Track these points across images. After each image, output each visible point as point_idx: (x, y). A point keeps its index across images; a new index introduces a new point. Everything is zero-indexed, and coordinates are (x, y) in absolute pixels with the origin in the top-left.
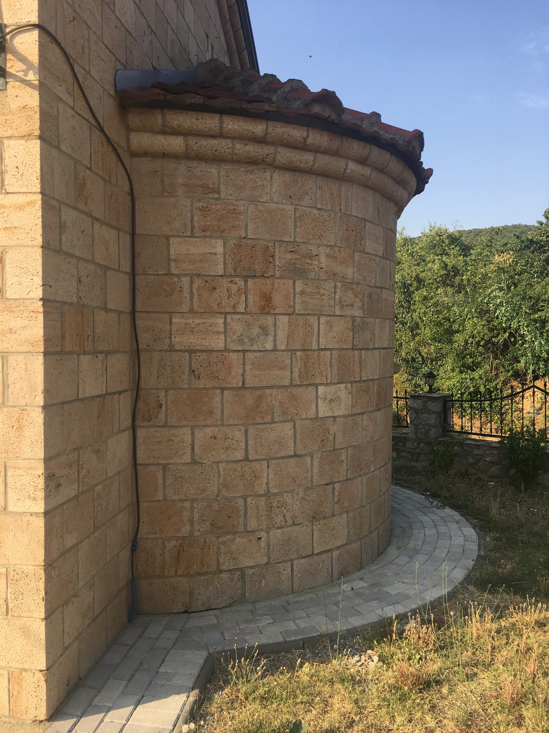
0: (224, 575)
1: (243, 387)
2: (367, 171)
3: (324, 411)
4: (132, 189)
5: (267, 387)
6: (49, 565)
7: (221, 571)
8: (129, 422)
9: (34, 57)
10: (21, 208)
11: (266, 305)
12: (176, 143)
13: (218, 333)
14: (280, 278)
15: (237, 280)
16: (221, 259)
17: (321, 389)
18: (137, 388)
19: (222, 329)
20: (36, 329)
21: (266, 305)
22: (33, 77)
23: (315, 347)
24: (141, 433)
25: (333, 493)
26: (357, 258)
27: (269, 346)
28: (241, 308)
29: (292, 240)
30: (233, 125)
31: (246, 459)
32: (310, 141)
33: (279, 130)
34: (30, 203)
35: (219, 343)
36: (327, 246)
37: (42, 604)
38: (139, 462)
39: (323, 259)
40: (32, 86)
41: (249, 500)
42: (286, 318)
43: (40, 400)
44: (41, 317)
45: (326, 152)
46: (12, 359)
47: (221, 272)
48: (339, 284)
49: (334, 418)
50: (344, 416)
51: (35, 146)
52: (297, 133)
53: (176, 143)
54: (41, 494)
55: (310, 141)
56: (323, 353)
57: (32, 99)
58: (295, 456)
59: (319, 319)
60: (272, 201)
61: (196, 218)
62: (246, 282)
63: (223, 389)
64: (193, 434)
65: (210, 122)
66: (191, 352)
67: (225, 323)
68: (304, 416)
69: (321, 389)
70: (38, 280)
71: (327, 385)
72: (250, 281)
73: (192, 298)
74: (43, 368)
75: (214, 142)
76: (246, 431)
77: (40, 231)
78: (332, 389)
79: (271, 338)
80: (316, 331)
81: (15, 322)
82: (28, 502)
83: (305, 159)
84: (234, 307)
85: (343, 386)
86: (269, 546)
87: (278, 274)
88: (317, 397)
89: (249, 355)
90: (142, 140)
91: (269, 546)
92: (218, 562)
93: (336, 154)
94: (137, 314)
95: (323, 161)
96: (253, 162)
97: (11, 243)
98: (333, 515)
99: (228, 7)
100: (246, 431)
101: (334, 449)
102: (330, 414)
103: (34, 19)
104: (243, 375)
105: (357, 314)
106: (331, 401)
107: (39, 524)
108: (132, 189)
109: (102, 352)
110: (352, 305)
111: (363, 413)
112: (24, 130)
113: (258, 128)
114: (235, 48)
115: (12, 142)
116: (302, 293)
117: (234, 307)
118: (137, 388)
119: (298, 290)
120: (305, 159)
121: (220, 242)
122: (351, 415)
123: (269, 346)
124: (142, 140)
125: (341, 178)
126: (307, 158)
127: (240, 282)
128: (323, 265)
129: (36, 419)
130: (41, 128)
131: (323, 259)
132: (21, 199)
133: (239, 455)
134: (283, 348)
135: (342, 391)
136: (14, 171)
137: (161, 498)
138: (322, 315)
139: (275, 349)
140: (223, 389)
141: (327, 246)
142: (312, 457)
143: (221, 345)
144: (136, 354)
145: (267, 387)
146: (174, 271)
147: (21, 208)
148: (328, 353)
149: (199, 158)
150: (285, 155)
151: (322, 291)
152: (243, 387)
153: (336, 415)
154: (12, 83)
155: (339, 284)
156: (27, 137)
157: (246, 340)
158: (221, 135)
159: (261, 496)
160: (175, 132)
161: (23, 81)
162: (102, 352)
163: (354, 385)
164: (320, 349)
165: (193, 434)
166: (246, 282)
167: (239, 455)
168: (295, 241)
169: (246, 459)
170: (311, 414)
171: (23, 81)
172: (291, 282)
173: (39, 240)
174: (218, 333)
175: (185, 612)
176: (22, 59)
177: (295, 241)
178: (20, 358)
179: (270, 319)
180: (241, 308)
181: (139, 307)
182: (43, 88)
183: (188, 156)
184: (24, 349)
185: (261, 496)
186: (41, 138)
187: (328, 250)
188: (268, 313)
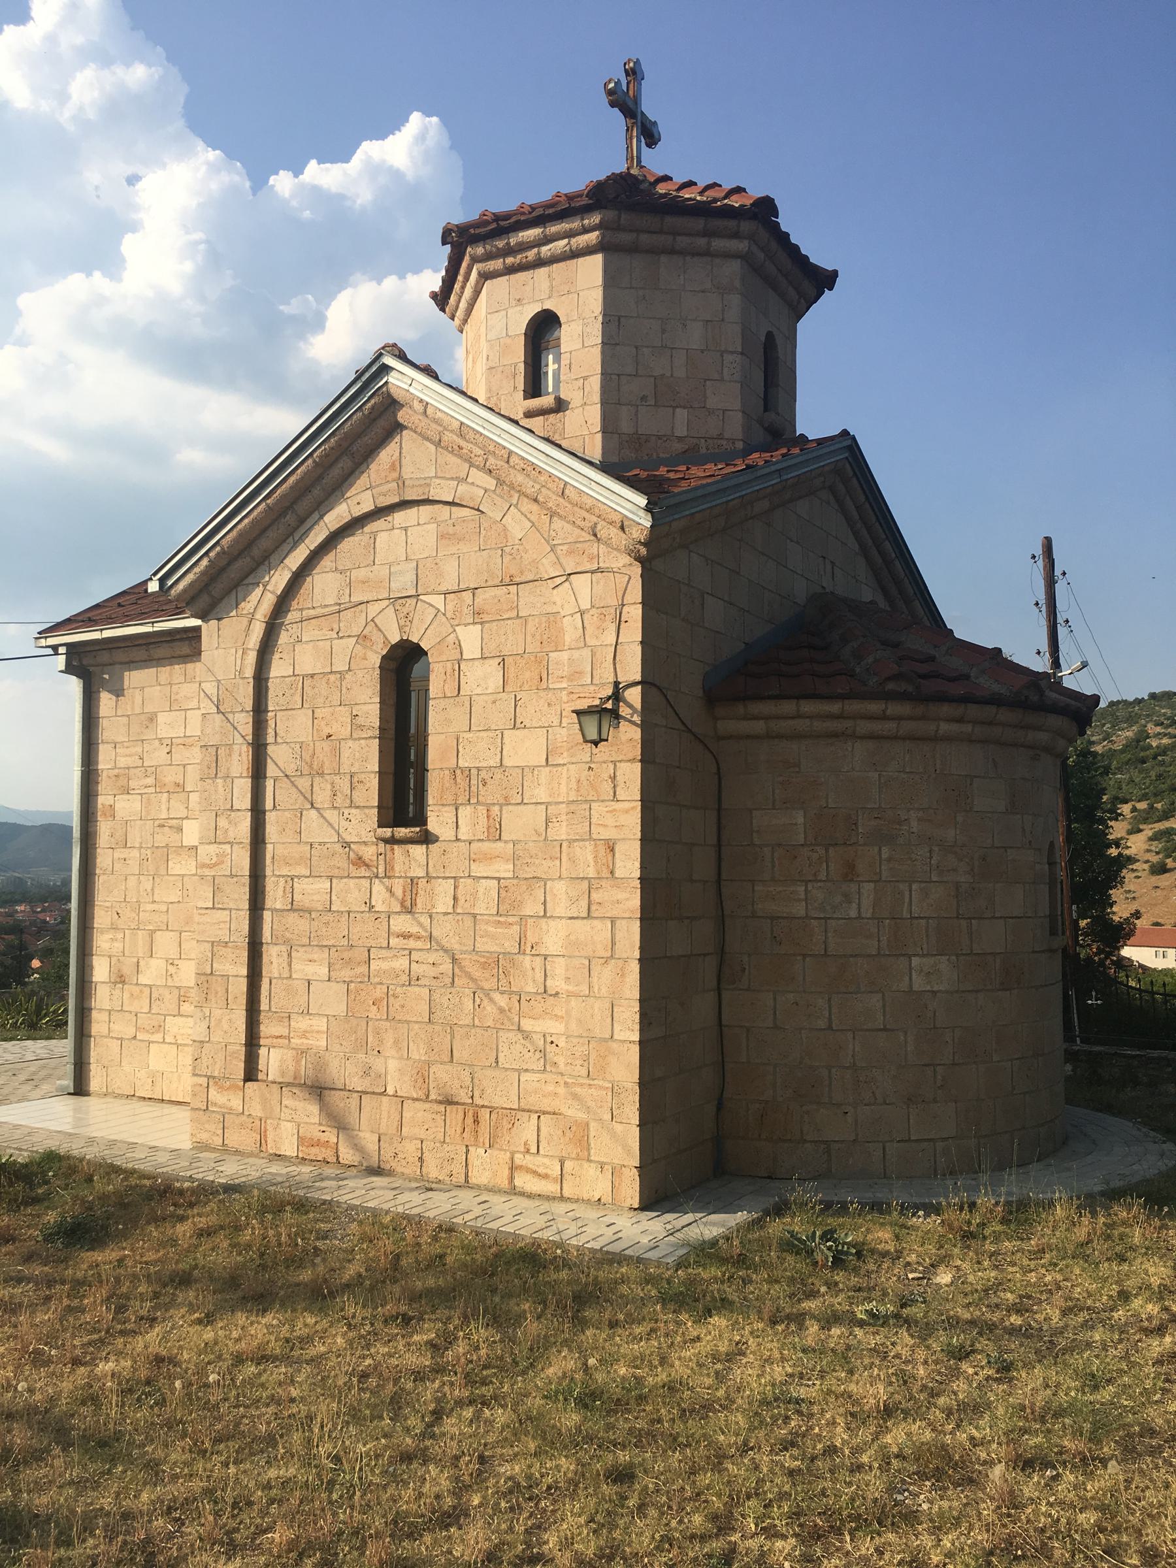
0: (807, 1145)
1: (826, 955)
2: (968, 728)
3: (919, 983)
4: (719, 769)
5: (851, 956)
6: (642, 1084)
7: (805, 1141)
8: (715, 983)
9: (638, 705)
10: (627, 812)
11: (849, 872)
12: (759, 727)
13: (799, 900)
14: (865, 845)
15: (818, 848)
16: (802, 830)
17: (915, 961)
18: (722, 952)
19: (803, 897)
20: (635, 901)
21: (849, 872)
22: (637, 719)
23: (906, 914)
24: (726, 995)
25: (935, 1077)
26: (960, 819)
27: (853, 913)
28: (822, 876)
29: (877, 806)
30: (808, 707)
31: (830, 1028)
32: (889, 712)
33: (855, 706)
34: (633, 808)
35: (800, 910)
36: (919, 809)
37: (637, 1113)
38: (724, 1022)
39: (914, 824)
40: (636, 725)
41: (834, 1070)
42: (872, 885)
43: (637, 954)
44: (639, 891)
45: (910, 718)
46: (618, 922)
47: (802, 841)
48: (936, 849)
49: (934, 992)
50: (947, 992)
51: (638, 766)
52: (874, 707)
53: (759, 727)
54: (637, 1027)
55: (889, 712)
56: (915, 922)
57: (636, 733)
58: (885, 1029)
59: (910, 886)
60: (853, 769)
61: (777, 791)
62: (827, 851)
63: (804, 956)
64: (775, 999)
65: (788, 707)
66: (772, 918)
67: (806, 890)
68: (894, 988)
69: (915, 961)
70: (638, 864)
71: (923, 956)
72: (831, 850)
73: (773, 867)
74: (623, 820)
75: (791, 722)
76: (829, 1000)
77: (639, 828)
78: (930, 961)
79: (854, 905)
80: (907, 900)
81: (621, 896)
82: (628, 1033)
83: (890, 727)
84: (815, 875)
85: (945, 958)
86: (856, 1121)
87: (861, 841)
88: (911, 969)
89: (833, 923)
90: (728, 726)
91: (856, 1121)
92: (802, 1131)
93: (923, 718)
94: (723, 883)
95: (908, 727)
96: (835, 735)
97: (619, 837)
98: (935, 1101)
99: (857, 507)
100: (829, 1000)
101: (935, 1028)
102: (928, 988)
103: (638, 678)
104: (825, 942)
105: (963, 880)
106: (928, 974)
107: (636, 1050)
108: (719, 769)
109: (688, 918)
110: (955, 870)
111: (977, 991)
112: (630, 756)
113: (835, 707)
114: (870, 542)
115: (622, 764)
116: (889, 860)
117: (815, 875)
118: (722, 952)
119: (884, 856)
120: (890, 727)
121: (801, 813)
122: (957, 992)
123: (853, 913)
124: (728, 726)
125: (935, 739)
126: (891, 726)
127: (821, 851)
128: (915, 830)
129: (635, 967)
130: (642, 754)
131: (914, 824)
132: (627, 805)
133: (822, 1024)
134: (869, 915)
135: (943, 963)
136: (622, 785)
137: (744, 1060)
138: (914, 882)
139: (860, 917)
140: (804, 956)
141: (919, 809)
142: (906, 1033)
143: (802, 913)
144: (721, 921)
145: (851, 956)
146: (757, 841)
147: (627, 812)
148: (923, 922)
149: (780, 736)
150: (864, 727)
151: (913, 856)
152: (826, 955)
153: (935, 989)
154: (622, 723)
155: (936, 849)
156: (632, 760)
157: (828, 908)
158: (799, 716)
159: (847, 1068)
160: (756, 718)
161: (630, 721)
162: (688, 918)
163: (962, 958)
164: (912, 918)
165: (775, 999)
166: (827, 851)
167: (822, 1024)
168: (880, 807)
169: (830, 1028)
170: (904, 986)
171: (630, 721)
172: (876, 849)
173: (639, 835)
174: (799, 900)
175: (770, 1177)
176: (630, 706)
177: (880, 807)
178: (624, 922)
179: (853, 887)
180: (822, 876)
181: (724, 876)
182: (645, 726)
183: (769, 736)
184: (627, 915)
185: (847, 1068)
186: (641, 761)
187: (920, 814)
188: (852, 880)
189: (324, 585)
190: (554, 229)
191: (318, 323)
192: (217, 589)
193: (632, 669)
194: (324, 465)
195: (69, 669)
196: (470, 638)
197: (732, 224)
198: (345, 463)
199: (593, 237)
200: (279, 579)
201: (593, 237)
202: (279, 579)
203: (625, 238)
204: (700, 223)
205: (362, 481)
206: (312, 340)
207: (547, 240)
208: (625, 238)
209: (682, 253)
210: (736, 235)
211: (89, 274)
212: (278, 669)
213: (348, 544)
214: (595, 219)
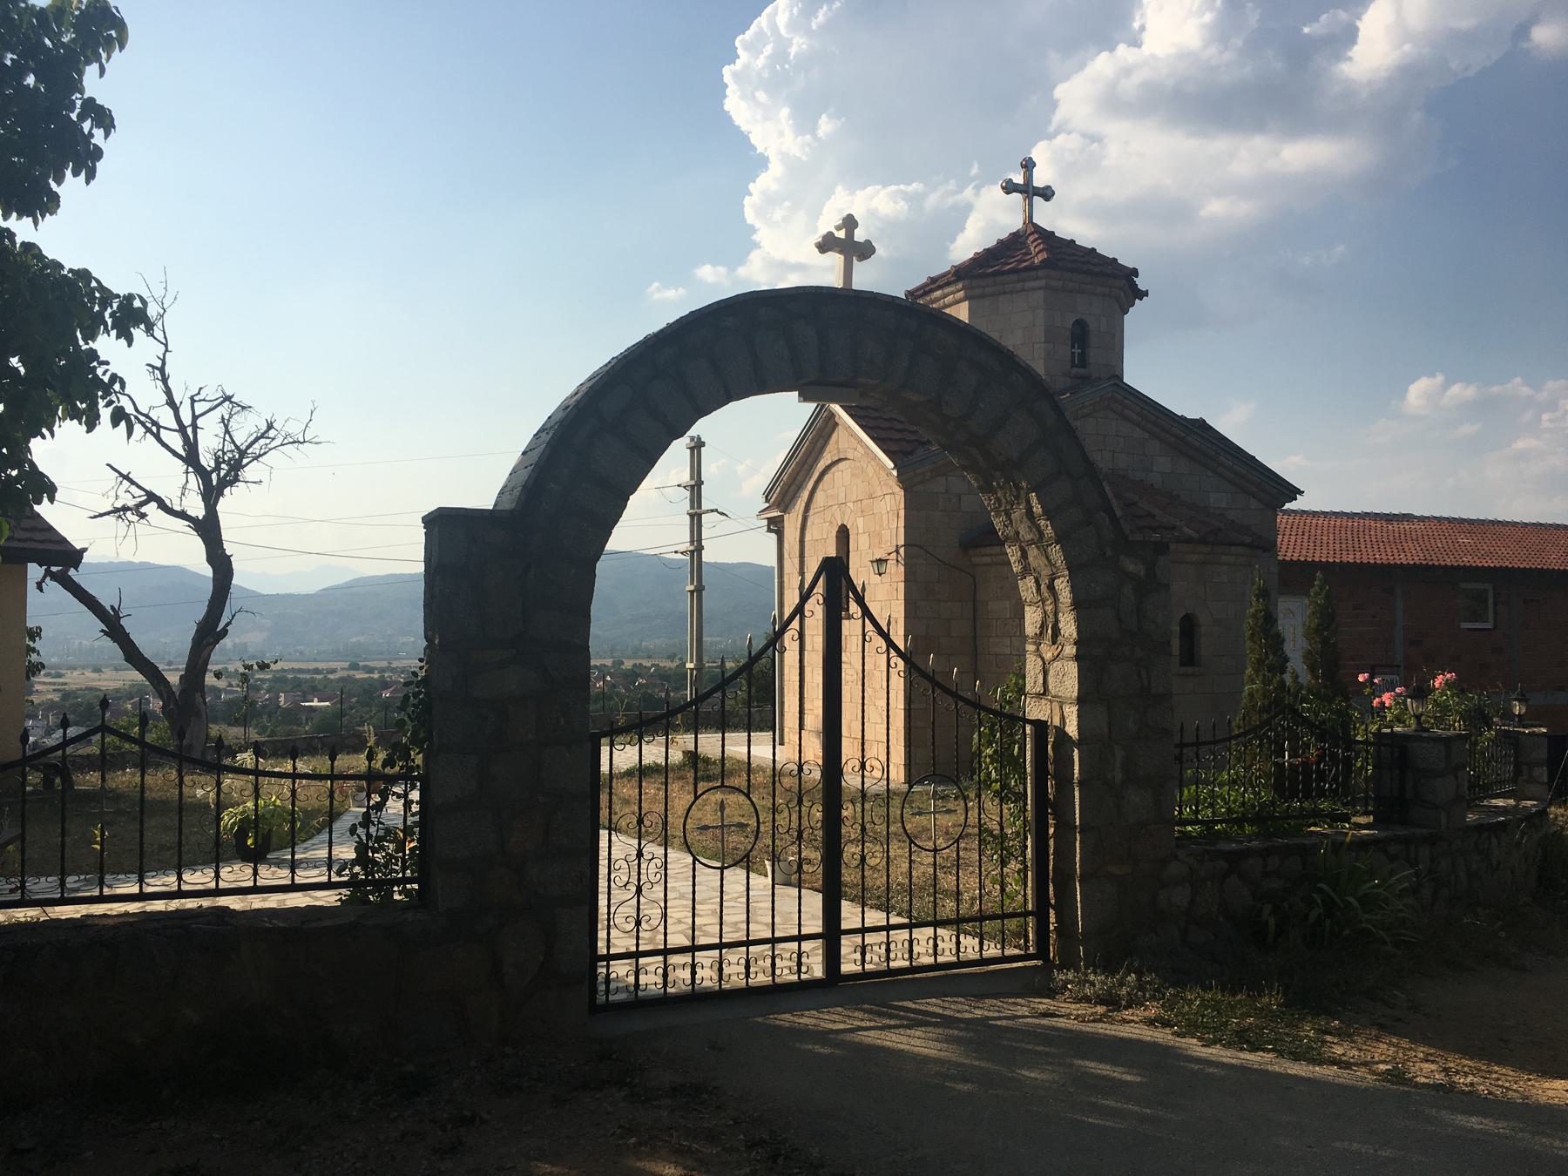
12: (988, 560)
53: (988, 560)
189: (820, 495)
190: (947, 290)
191: (1349, 35)
192: (787, 499)
193: (902, 542)
194: (813, 443)
195: (769, 530)
196: (860, 521)
197: (1033, 273)
198: (821, 441)
199: (961, 294)
200: (805, 494)
201: (961, 294)
202: (805, 494)
203: (978, 292)
204: (1014, 277)
205: (828, 449)
206: (1350, 54)
207: (946, 296)
208: (978, 292)
209: (1011, 292)
210: (1037, 278)
211: (1112, 49)
212: (807, 538)
213: (827, 477)
214: (960, 285)
